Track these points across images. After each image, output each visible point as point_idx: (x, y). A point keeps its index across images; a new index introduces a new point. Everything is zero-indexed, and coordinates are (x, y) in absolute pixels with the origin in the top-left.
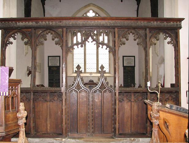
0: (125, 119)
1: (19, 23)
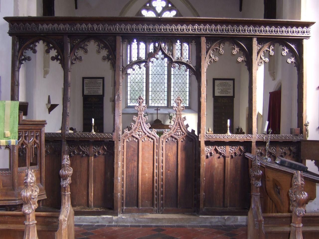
0: (215, 185)
1: (42, 25)
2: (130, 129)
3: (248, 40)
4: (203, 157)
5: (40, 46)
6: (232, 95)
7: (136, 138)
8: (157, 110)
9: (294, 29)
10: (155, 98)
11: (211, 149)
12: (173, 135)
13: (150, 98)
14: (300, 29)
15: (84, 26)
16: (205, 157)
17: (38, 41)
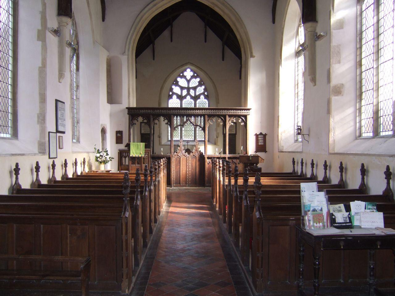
2: (177, 153)
3: (225, 116)
4: (206, 164)
6: (234, 133)
7: (179, 156)
8: (188, 143)
9: (243, 111)
10: (186, 135)
11: (210, 160)
12: (194, 155)
13: (183, 135)
14: (246, 111)
16: (207, 164)
17: (139, 117)
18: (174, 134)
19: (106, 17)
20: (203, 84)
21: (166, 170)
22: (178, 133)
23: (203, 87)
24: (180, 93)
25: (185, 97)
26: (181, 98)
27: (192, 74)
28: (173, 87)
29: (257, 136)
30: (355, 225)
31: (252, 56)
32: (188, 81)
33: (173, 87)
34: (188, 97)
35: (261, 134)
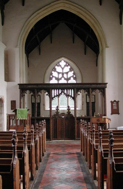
5: (28, 92)
15: (41, 86)
18: (52, 103)
19: (5, 22)
20: (73, 70)
21: (45, 129)
22: (56, 102)
23: (73, 72)
24: (57, 77)
25: (61, 79)
26: (58, 79)
27: (65, 64)
28: (53, 72)
29: (112, 103)
30: (52, 110)
31: (107, 47)
32: (63, 69)
33: (53, 72)
34: (63, 79)
35: (115, 101)
